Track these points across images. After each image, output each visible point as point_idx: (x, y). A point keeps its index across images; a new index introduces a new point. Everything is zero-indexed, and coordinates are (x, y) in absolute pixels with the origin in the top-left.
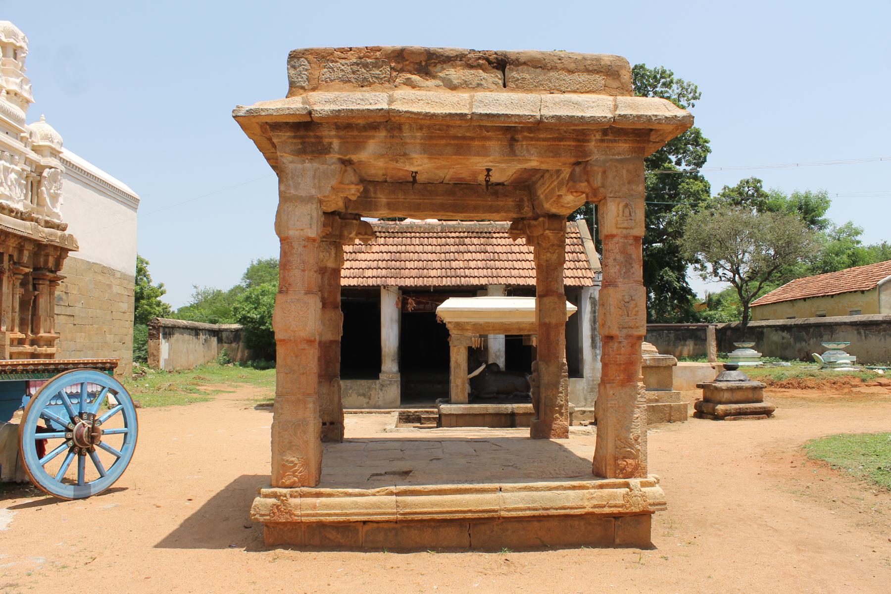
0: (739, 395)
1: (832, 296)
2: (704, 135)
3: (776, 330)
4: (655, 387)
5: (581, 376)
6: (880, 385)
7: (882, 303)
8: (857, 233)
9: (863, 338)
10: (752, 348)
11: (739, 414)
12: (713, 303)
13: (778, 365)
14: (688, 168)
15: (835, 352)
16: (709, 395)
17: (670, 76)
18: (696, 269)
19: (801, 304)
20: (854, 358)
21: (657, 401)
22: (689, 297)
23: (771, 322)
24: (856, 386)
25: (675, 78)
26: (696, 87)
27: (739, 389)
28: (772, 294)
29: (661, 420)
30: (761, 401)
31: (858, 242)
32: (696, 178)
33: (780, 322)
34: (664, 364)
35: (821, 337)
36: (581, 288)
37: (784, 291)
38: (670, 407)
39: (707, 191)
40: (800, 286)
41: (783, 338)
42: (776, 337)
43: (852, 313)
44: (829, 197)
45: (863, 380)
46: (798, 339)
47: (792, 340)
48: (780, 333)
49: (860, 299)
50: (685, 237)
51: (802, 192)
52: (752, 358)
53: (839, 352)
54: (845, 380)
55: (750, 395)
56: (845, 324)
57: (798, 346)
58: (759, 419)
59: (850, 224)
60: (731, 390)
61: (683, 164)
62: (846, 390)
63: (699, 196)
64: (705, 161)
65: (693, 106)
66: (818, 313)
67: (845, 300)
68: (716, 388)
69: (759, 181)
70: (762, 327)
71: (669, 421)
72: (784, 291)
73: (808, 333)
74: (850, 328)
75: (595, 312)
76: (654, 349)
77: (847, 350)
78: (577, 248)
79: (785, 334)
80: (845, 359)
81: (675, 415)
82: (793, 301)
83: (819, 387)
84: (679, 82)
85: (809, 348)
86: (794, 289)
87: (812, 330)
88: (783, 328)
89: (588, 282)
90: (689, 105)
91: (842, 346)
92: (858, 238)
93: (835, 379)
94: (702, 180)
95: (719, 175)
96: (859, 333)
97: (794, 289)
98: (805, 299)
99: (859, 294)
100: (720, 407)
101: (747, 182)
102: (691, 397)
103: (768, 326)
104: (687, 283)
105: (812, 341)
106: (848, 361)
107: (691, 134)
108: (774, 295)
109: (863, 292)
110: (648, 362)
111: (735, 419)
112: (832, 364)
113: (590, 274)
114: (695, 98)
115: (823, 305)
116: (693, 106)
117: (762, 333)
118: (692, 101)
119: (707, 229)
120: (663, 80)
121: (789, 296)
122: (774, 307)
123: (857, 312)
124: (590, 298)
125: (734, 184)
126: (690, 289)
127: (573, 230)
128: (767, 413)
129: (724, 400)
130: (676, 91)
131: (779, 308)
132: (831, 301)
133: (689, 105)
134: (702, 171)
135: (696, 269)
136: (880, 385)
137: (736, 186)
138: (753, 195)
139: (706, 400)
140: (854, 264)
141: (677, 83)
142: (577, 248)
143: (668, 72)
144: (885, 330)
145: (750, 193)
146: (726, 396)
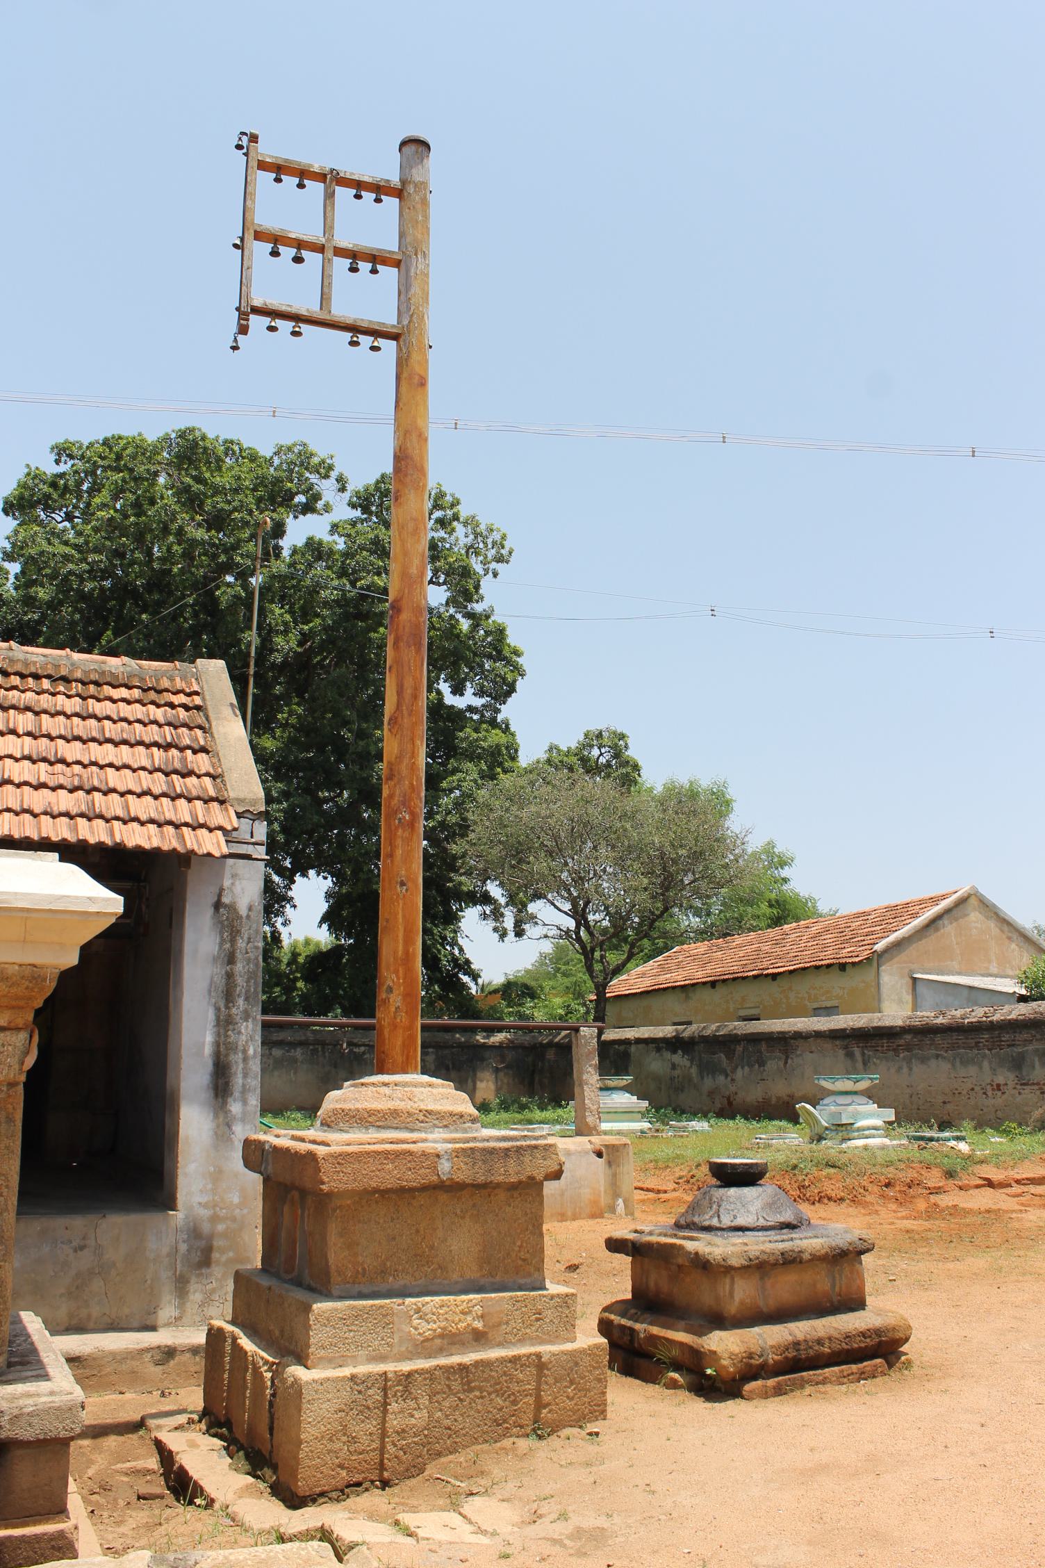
0: (785, 1288)
1: (774, 976)
2: (512, 639)
3: (658, 1050)
4: (473, 1273)
5: (169, 1203)
6: (990, 1184)
7: (885, 990)
8: (783, 863)
9: (860, 1065)
10: (625, 1089)
11: (796, 1367)
12: (517, 991)
13: (684, 1129)
14: (478, 702)
15: (848, 1099)
16: (658, 1280)
17: (452, 506)
18: (484, 916)
19: (706, 995)
20: (890, 1115)
21: (479, 1338)
22: (465, 979)
23: (645, 1032)
24: (937, 1191)
25: (464, 511)
26: (504, 537)
27: (790, 1261)
28: (636, 978)
29: (500, 1428)
30: (856, 1303)
31: (785, 880)
32: (493, 723)
33: (667, 1031)
34: (509, 1172)
35: (762, 1063)
36: (184, 860)
37: (663, 969)
38: (540, 1364)
39: (512, 751)
40: (694, 958)
41: (674, 1067)
42: (657, 1064)
43: (817, 1012)
44: (731, 793)
45: (950, 1174)
46: (708, 1069)
47: (694, 1071)
48: (667, 1055)
49: (837, 985)
50: (472, 836)
51: (683, 780)
52: (627, 1113)
53: (856, 1098)
54: (912, 1174)
55: (822, 1282)
56: (818, 1035)
57: (708, 1083)
58: (863, 1376)
59: (770, 845)
60: (760, 1267)
61: (469, 690)
62: (921, 1205)
63: (499, 758)
64: (512, 689)
65: (495, 575)
66: (742, 1013)
67: (802, 988)
68: (702, 1264)
69: (622, 737)
70: (627, 1042)
71: (541, 1430)
72: (663, 969)
73: (730, 1056)
74: (828, 1045)
75: (231, 959)
76: (461, 1103)
77: (869, 1094)
78: (185, 736)
79: (678, 1058)
80: (871, 1116)
81: (559, 1397)
82: (686, 989)
83: (854, 1198)
84: (471, 522)
85: (733, 1089)
86: (686, 963)
87: (739, 1049)
88: (674, 1044)
89: (212, 844)
90: (486, 571)
91: (864, 1085)
92: (785, 872)
93: (891, 1172)
94: (506, 729)
95: (538, 723)
96: (850, 1055)
97: (686, 963)
98: (713, 984)
99: (836, 970)
100: (725, 1345)
101: (600, 735)
102: (586, 1284)
103: (639, 1041)
104: (461, 950)
105: (739, 1072)
106: (879, 1123)
107: (487, 633)
108: (643, 975)
109: (843, 967)
110: (445, 1167)
111: (779, 1391)
112: (843, 1129)
113: (217, 816)
114: (500, 559)
115: (753, 996)
116: (495, 575)
117: (626, 1056)
118: (493, 565)
119: (524, 814)
120: (438, 514)
121: (677, 977)
122: (645, 1002)
123: (829, 1011)
124: (218, 905)
125: (569, 740)
126: (468, 962)
127: (179, 684)
128: (882, 1351)
129: (732, 1308)
130: (463, 541)
131: (656, 1003)
132: (774, 987)
133: (486, 571)
134: (507, 711)
135: (484, 916)
136: (990, 1184)
137: (574, 745)
138: (608, 765)
139: (646, 1302)
140: (777, 921)
141: (466, 524)
142: (185, 736)
143: (449, 498)
144: (909, 1048)
145: (602, 760)
146: (741, 1293)
